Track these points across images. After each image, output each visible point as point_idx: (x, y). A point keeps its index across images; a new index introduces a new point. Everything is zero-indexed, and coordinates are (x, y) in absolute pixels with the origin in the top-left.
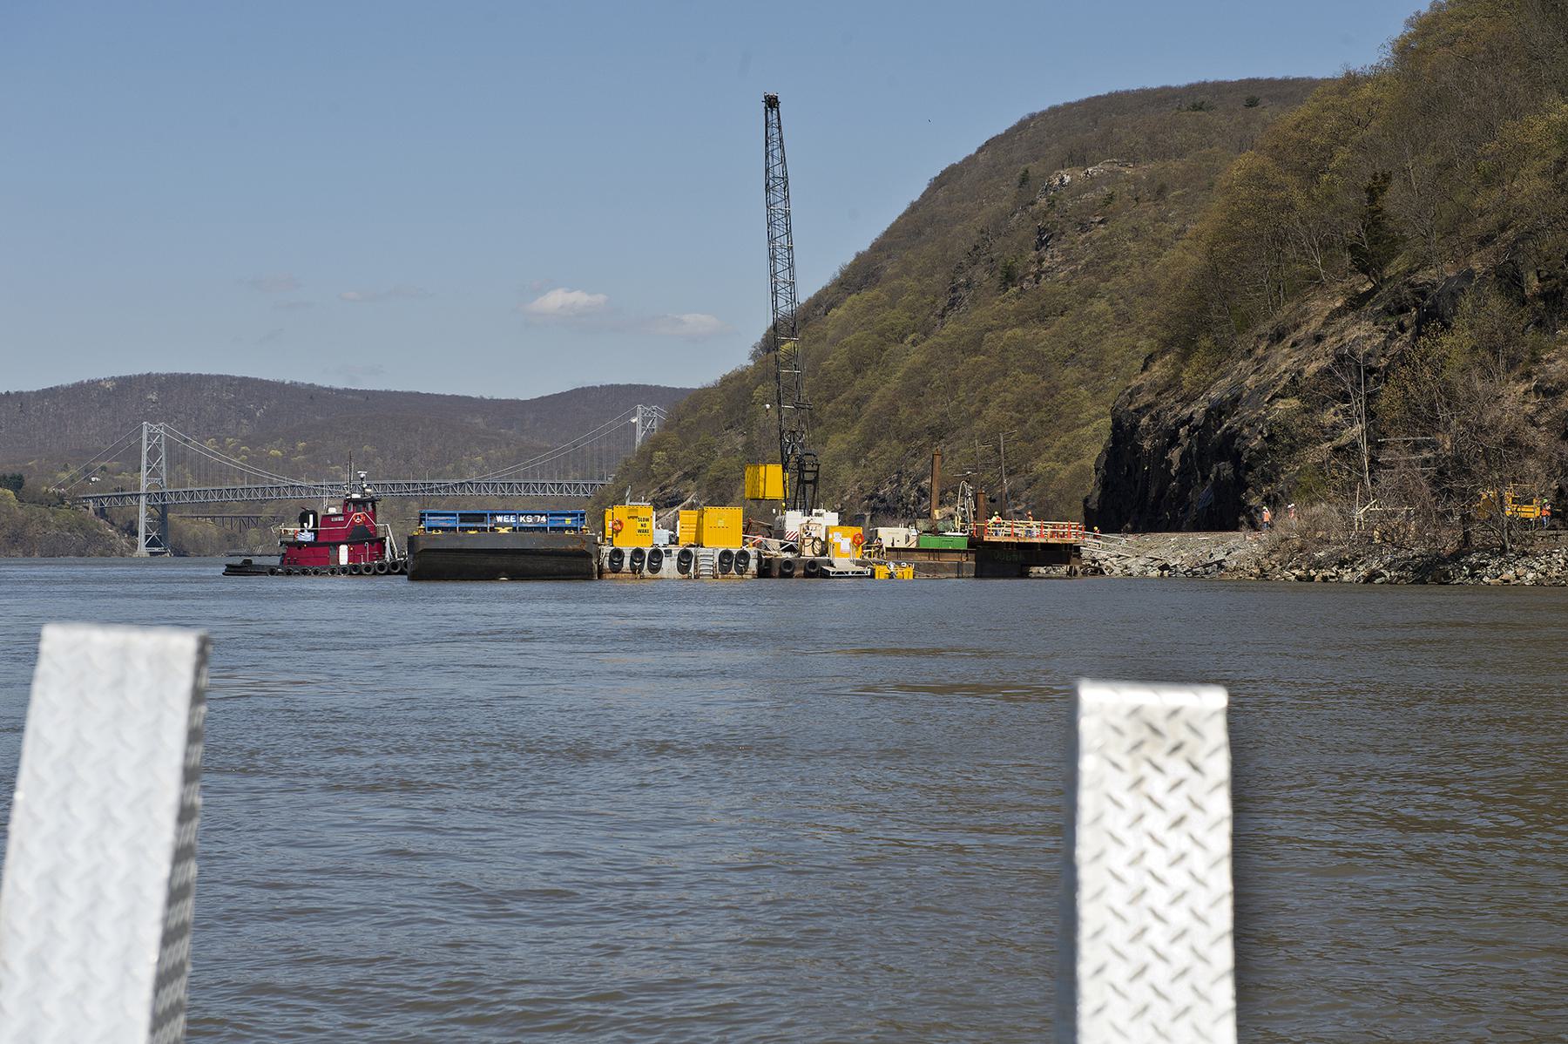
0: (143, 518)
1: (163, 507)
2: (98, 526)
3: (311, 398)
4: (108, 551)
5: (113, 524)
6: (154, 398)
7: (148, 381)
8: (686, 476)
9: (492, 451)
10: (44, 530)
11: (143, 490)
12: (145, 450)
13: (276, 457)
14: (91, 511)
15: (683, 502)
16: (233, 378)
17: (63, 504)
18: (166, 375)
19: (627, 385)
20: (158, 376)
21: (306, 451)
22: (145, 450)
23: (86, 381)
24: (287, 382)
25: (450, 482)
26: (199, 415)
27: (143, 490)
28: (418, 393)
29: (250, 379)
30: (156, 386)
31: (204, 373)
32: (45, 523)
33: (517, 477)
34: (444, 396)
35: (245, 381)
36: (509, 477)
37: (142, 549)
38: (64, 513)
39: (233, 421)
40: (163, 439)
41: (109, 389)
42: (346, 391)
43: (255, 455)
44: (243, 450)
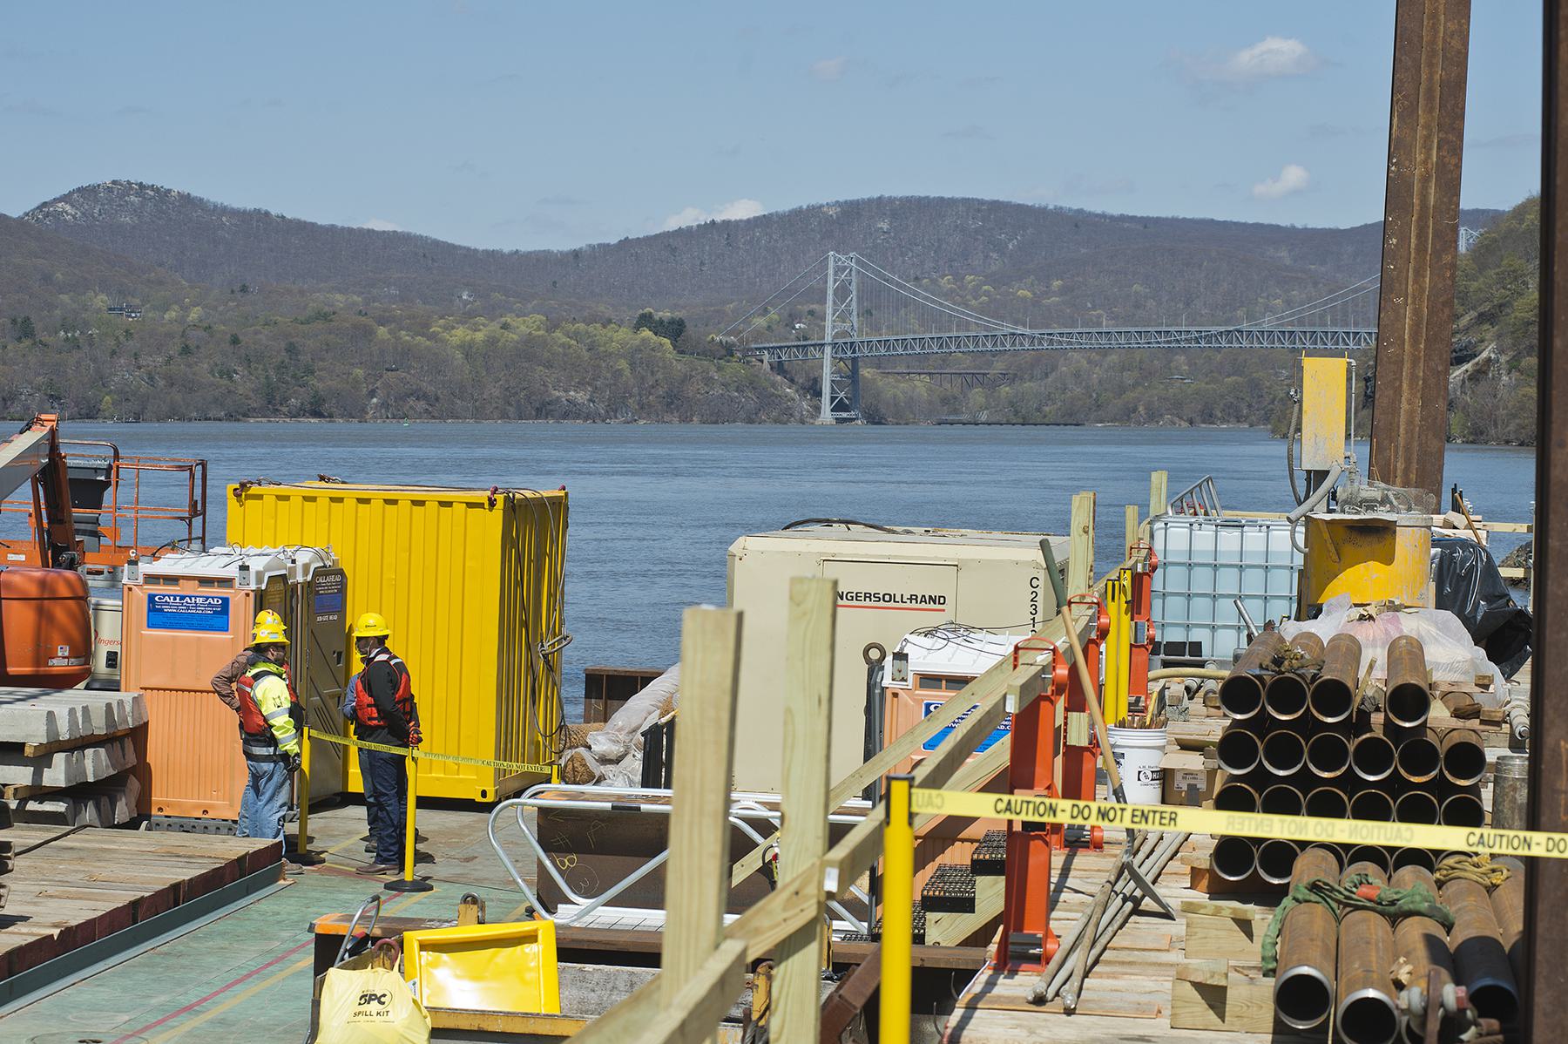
0: (828, 374)
1: (854, 360)
2: (774, 385)
3: (1076, 226)
4: (785, 415)
5: (792, 381)
6: (885, 227)
7: (880, 206)
8: (1483, 318)
9: (1294, 292)
10: (706, 389)
11: (828, 339)
12: (831, 287)
13: (1024, 299)
14: (766, 366)
15: (1476, 356)
16: (981, 202)
17: (732, 356)
18: (901, 199)
19: (1473, 210)
20: (891, 200)
21: (1063, 291)
22: (831, 287)
23: (805, 207)
24: (1051, 207)
25: (1214, 329)
26: (939, 247)
27: (828, 339)
28: (1212, 220)
29: (1002, 203)
30: (888, 213)
31: (947, 195)
32: (708, 381)
33: (1301, 322)
34: (1245, 224)
35: (996, 206)
36: (1291, 324)
37: (827, 415)
38: (734, 368)
39: (980, 254)
40: (853, 273)
41: (831, 216)
42: (1123, 218)
43: (998, 297)
44: (985, 291)
